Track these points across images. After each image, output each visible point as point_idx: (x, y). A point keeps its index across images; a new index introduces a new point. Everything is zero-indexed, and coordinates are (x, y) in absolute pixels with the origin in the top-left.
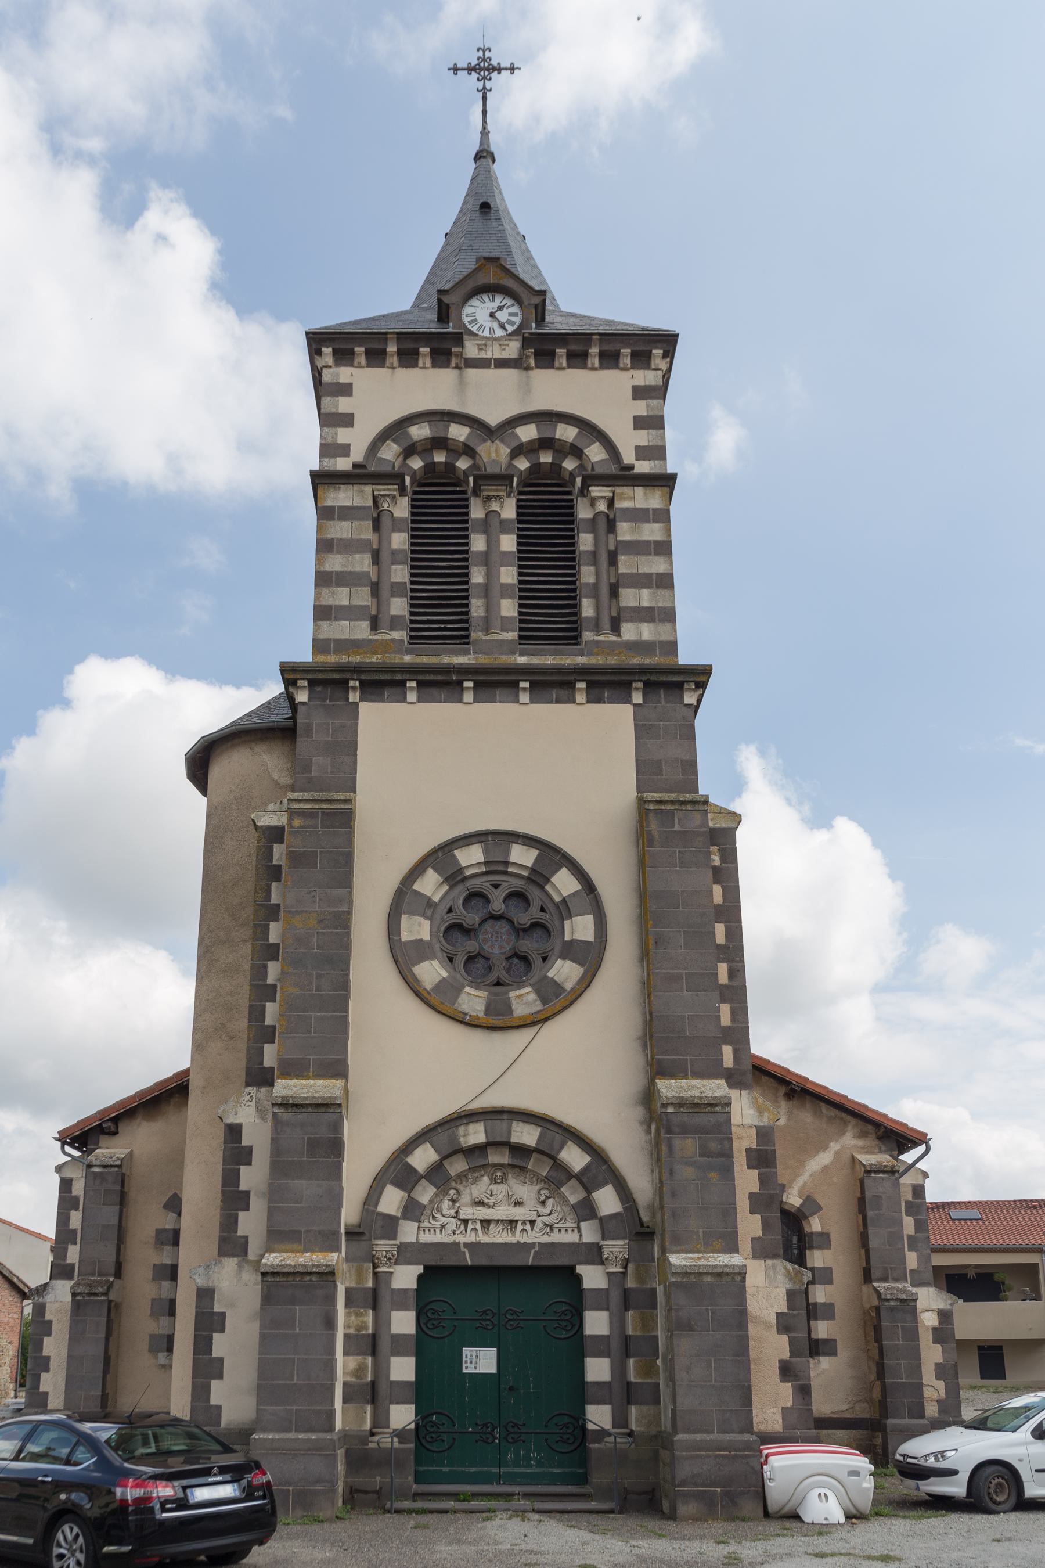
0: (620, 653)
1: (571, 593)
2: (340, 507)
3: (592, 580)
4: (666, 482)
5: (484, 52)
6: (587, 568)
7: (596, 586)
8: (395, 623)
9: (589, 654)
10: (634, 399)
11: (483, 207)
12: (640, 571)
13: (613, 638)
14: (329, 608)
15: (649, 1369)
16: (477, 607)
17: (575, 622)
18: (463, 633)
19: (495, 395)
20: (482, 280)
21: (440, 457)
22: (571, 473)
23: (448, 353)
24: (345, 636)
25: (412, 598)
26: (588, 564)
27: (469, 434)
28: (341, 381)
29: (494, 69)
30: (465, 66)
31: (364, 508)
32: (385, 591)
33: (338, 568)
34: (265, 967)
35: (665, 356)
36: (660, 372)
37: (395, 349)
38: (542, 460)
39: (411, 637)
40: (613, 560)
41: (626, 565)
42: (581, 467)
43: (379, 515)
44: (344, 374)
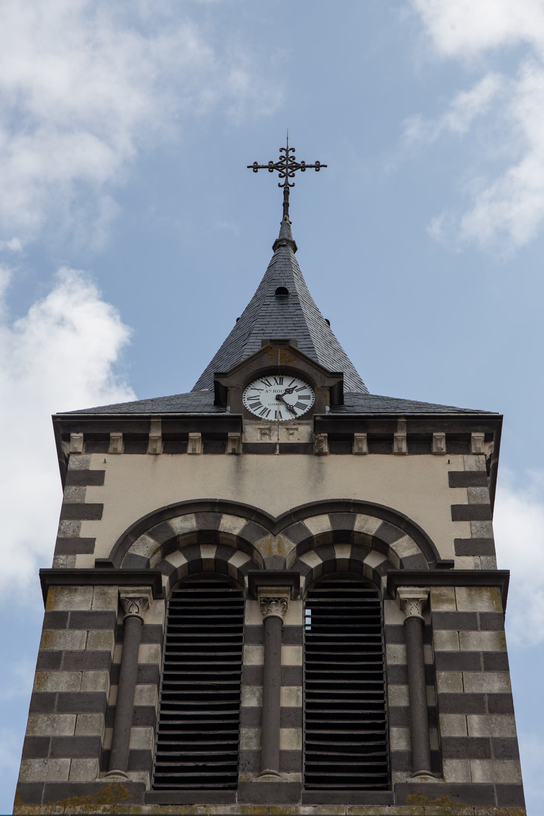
0: (443, 801)
1: (378, 719)
2: (74, 613)
3: (403, 703)
4: (499, 581)
5: (287, 151)
6: (396, 687)
7: (408, 711)
8: (135, 760)
9: (400, 802)
10: (451, 486)
11: (280, 291)
12: (467, 691)
13: (432, 780)
14: (46, 740)
16: (248, 739)
17: (383, 758)
18: (229, 774)
19: (278, 484)
20: (267, 362)
21: (208, 554)
22: (375, 571)
23: (224, 439)
24: (64, 779)
25: (162, 727)
26: (398, 683)
27: (246, 526)
28: (91, 468)
29: (298, 167)
30: (267, 164)
31: (105, 613)
32: (124, 718)
33: (63, 688)
35: (487, 440)
36: (482, 458)
37: (159, 434)
38: (338, 556)
39: (157, 780)
40: (430, 678)
41: (447, 683)
42: (388, 564)
43: (124, 622)
44: (95, 461)
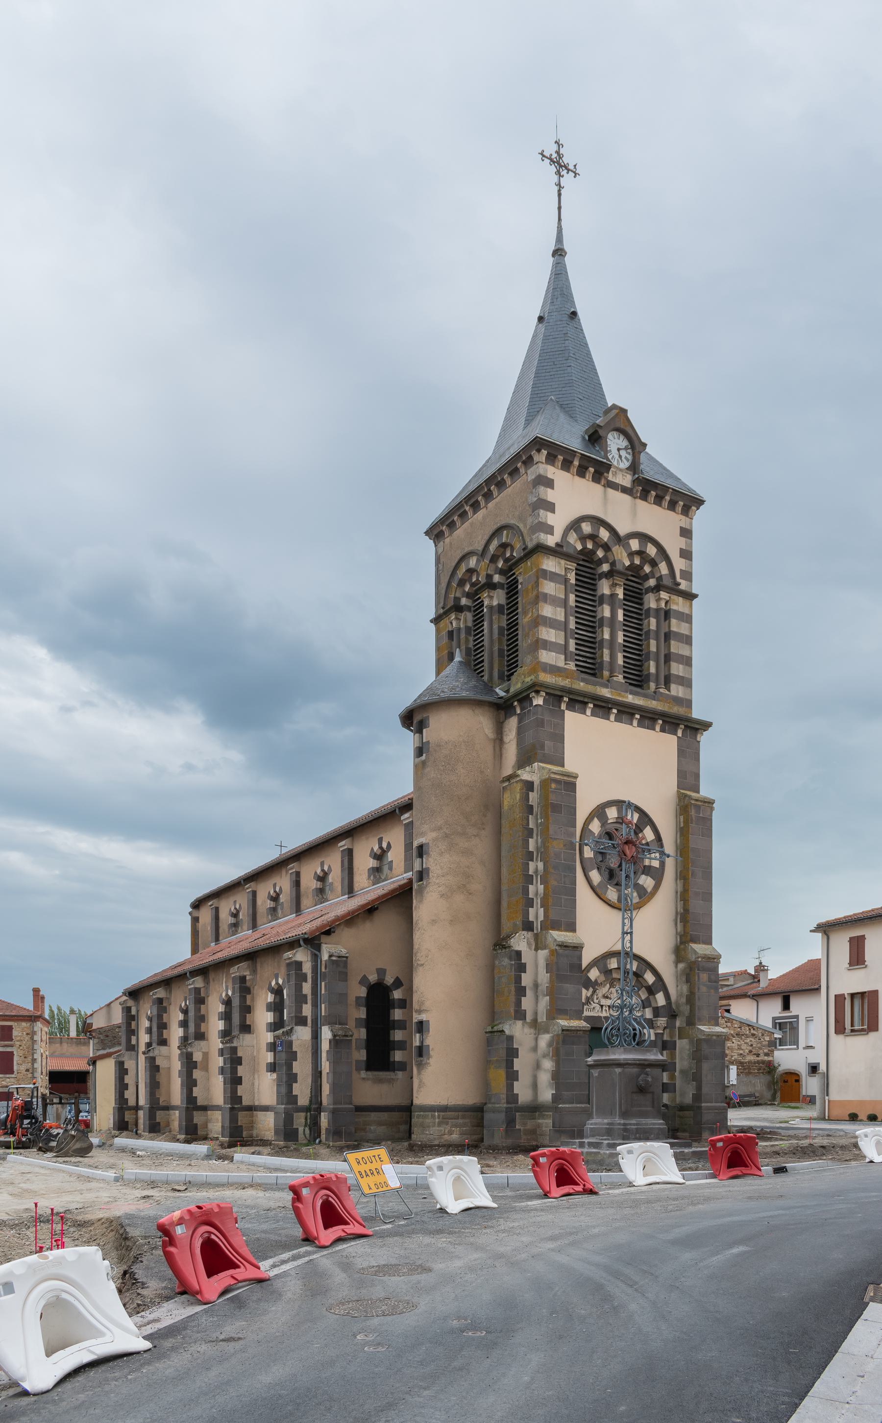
15: (672, 1077)
34: (528, 864)
